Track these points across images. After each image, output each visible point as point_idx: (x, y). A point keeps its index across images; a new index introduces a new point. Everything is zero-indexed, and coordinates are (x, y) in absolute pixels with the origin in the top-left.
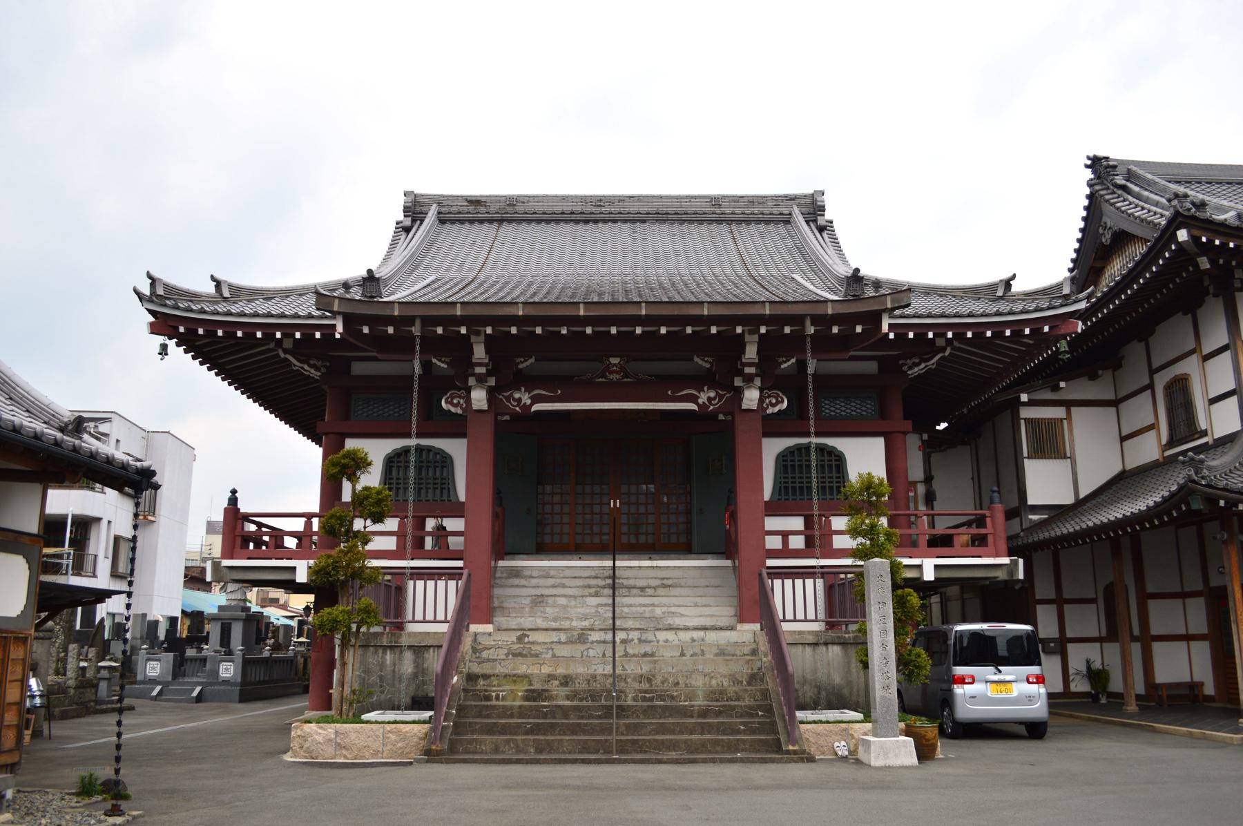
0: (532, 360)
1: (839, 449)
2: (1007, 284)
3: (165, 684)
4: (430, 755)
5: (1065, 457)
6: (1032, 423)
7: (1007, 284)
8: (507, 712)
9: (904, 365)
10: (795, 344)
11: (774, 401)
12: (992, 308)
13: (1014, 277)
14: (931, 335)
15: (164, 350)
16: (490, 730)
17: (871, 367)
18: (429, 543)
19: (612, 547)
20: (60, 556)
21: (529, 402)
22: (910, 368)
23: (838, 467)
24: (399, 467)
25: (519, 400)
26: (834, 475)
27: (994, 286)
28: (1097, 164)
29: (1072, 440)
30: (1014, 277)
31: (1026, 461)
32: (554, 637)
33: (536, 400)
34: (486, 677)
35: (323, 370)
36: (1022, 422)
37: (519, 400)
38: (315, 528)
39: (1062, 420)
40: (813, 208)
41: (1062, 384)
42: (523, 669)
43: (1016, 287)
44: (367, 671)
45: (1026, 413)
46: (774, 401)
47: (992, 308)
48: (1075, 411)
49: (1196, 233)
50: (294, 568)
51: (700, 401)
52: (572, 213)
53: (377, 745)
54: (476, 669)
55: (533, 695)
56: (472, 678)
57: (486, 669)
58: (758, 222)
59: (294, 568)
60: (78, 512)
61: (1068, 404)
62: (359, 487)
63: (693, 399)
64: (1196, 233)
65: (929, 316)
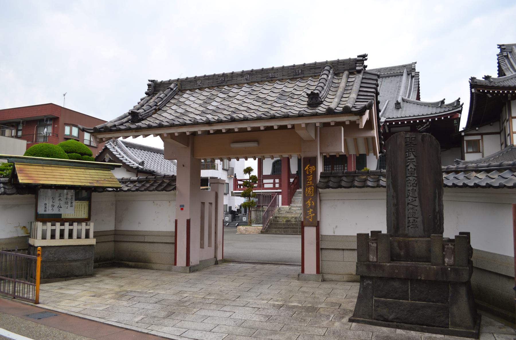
2: (443, 102)
3: (230, 223)
4: (262, 232)
5: (480, 152)
7: (443, 102)
8: (280, 224)
12: (439, 110)
13: (444, 99)
16: (276, 228)
20: (207, 189)
27: (438, 103)
28: (500, 46)
29: (483, 147)
30: (444, 99)
31: (466, 154)
32: (297, 208)
34: (279, 217)
40: (411, 71)
41: (477, 129)
42: (288, 216)
43: (447, 102)
44: (257, 216)
47: (439, 110)
48: (484, 136)
49: (479, 89)
53: (253, 231)
54: (278, 215)
55: (287, 221)
56: (276, 217)
57: (280, 215)
58: (392, 76)
60: (211, 176)
61: (482, 135)
62: (251, 175)
65: (410, 116)
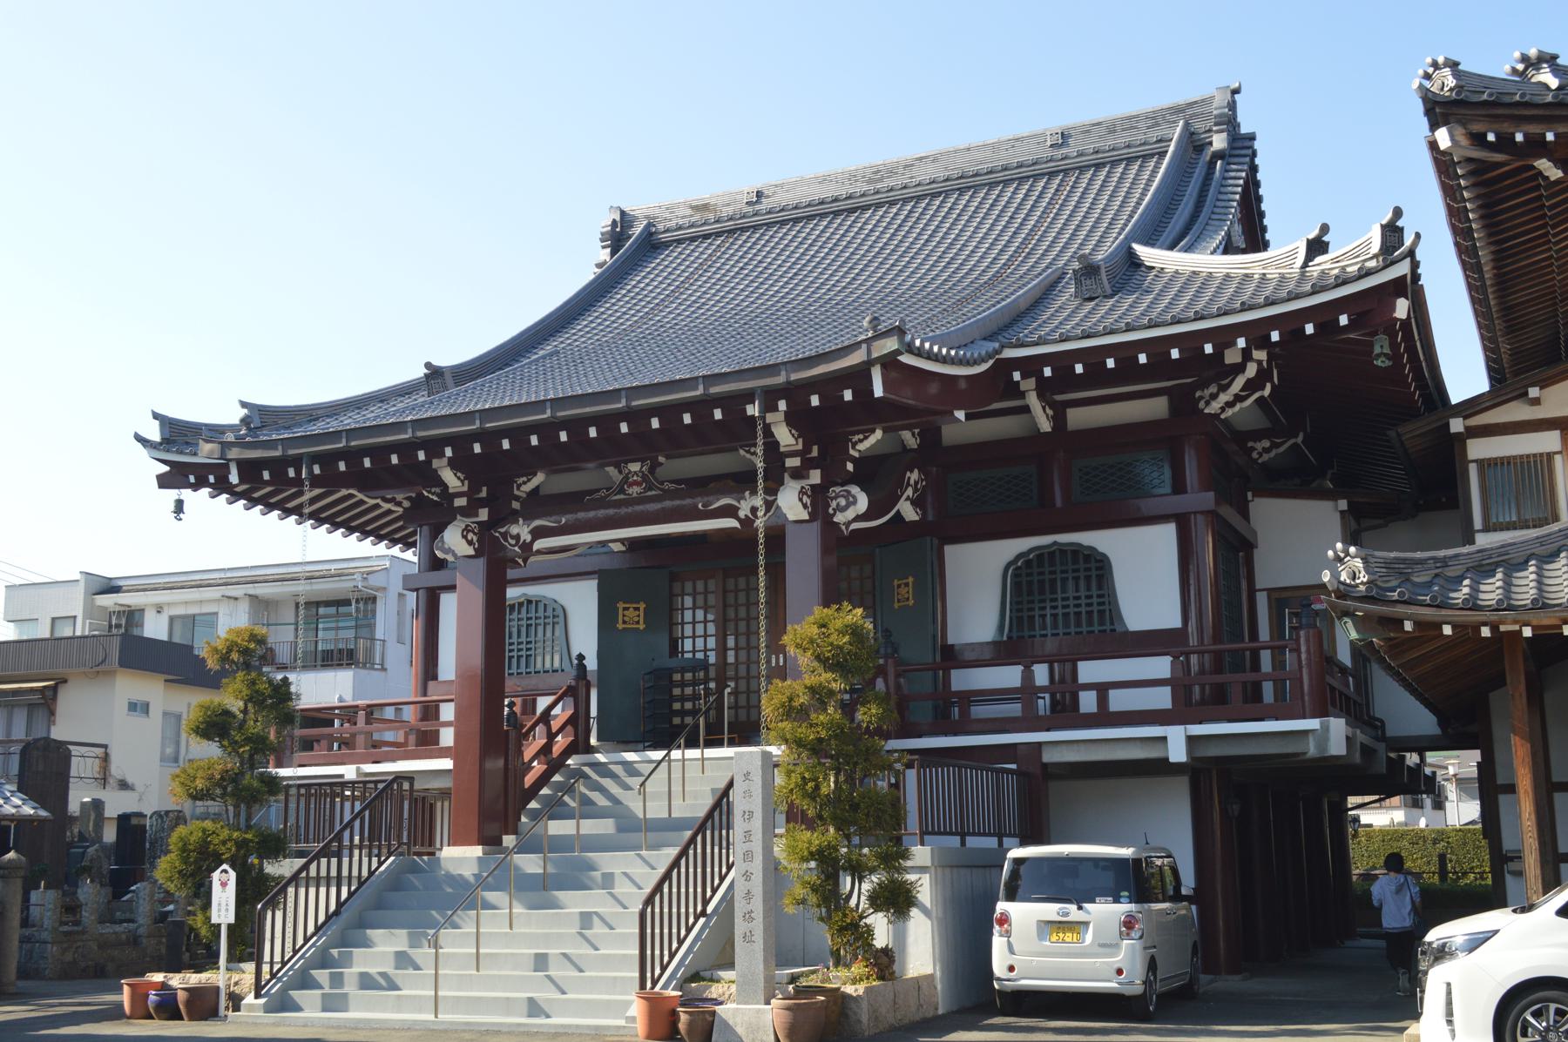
0: (878, 434)
1: (1101, 549)
6: (1484, 464)
9: (1201, 398)
10: (869, 412)
11: (843, 502)
14: (1208, 349)
15: (179, 507)
17: (1156, 408)
18: (1268, 690)
19: (68, 777)
21: (529, 538)
22: (1208, 403)
23: (1100, 578)
24: (1076, 579)
25: (517, 537)
26: (1094, 592)
30: (1398, 213)
33: (538, 533)
35: (406, 504)
36: (1473, 471)
37: (517, 537)
38: (1195, 667)
39: (1550, 456)
45: (1479, 449)
46: (843, 502)
50: (1164, 739)
51: (742, 514)
52: (836, 200)
59: (1164, 739)
63: (730, 511)
64: (1477, 128)
